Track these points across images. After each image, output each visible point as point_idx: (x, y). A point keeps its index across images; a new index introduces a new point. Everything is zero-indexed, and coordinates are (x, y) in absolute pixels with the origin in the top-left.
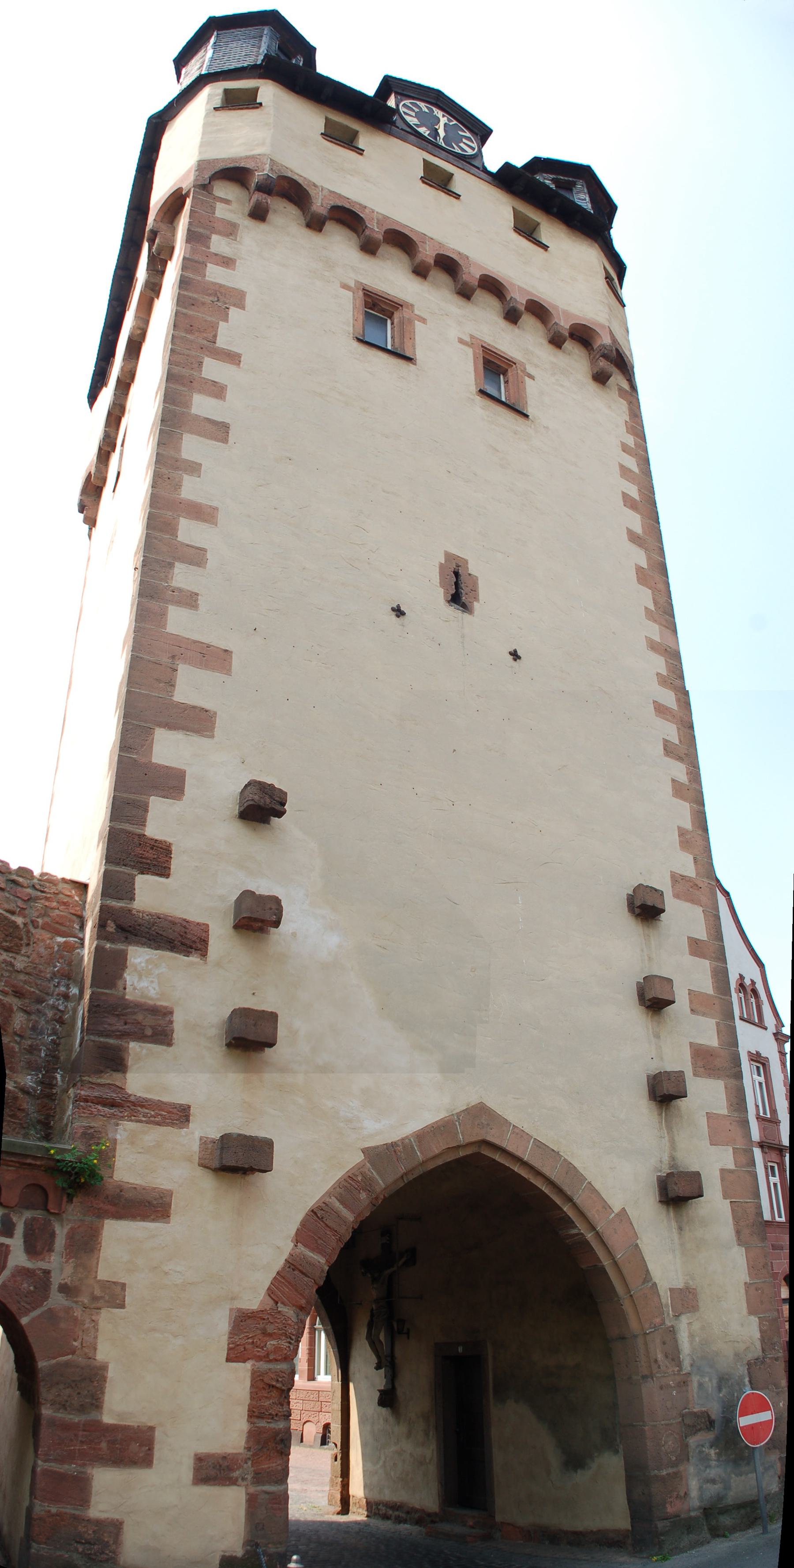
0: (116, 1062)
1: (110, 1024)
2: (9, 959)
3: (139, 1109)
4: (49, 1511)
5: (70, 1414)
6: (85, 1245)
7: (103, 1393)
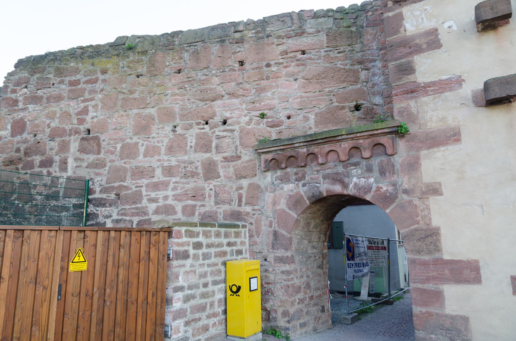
0: (408, 69)
1: (400, 53)
2: (351, 49)
3: (428, 89)
4: (421, 311)
5: (422, 255)
6: (413, 166)
7: (440, 242)
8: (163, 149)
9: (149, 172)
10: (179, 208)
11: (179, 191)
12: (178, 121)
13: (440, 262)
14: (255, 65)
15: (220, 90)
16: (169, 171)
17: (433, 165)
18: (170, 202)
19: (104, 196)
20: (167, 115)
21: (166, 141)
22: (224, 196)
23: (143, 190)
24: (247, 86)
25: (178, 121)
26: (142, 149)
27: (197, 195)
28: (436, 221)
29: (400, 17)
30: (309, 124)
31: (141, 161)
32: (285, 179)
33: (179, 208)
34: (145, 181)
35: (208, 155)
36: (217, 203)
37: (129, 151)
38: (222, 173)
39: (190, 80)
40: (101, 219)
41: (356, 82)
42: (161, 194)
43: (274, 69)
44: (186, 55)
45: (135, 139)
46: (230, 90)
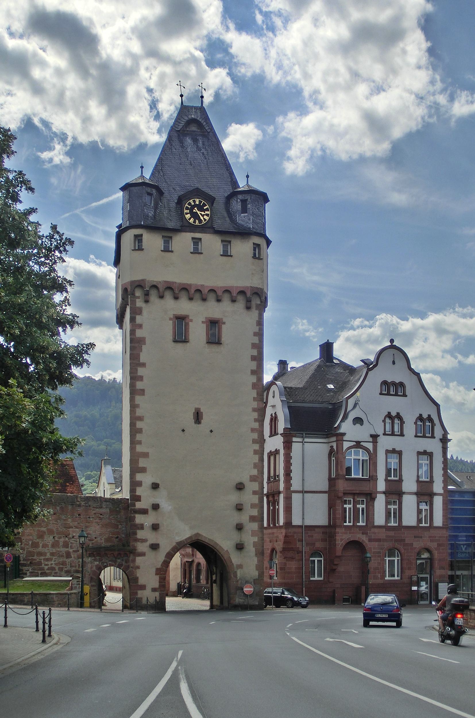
0: (136, 534)
6: (134, 561)
8: (50, 546)
9: (45, 554)
10: (57, 568)
11: (57, 562)
12: (55, 535)
13: (138, 586)
14: (84, 517)
15: (71, 524)
16: (52, 554)
17: (139, 560)
18: (53, 566)
19: (25, 562)
20: (51, 532)
21: (51, 542)
22: (73, 564)
23: (42, 561)
24: (82, 524)
25: (55, 535)
26: (41, 545)
27: (64, 563)
28: (138, 575)
29: (135, 517)
30: (101, 541)
31: (40, 549)
32: (95, 560)
33: (57, 568)
34: (42, 558)
35: (67, 549)
36: (71, 567)
37: (35, 545)
38: (72, 556)
39: (60, 519)
40: (24, 571)
41: (118, 528)
42: (50, 563)
43: (91, 519)
44: (58, 508)
45: (38, 540)
46: (75, 525)
